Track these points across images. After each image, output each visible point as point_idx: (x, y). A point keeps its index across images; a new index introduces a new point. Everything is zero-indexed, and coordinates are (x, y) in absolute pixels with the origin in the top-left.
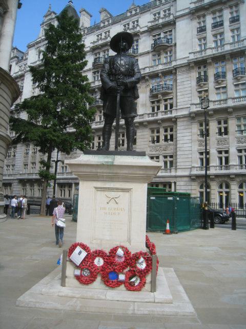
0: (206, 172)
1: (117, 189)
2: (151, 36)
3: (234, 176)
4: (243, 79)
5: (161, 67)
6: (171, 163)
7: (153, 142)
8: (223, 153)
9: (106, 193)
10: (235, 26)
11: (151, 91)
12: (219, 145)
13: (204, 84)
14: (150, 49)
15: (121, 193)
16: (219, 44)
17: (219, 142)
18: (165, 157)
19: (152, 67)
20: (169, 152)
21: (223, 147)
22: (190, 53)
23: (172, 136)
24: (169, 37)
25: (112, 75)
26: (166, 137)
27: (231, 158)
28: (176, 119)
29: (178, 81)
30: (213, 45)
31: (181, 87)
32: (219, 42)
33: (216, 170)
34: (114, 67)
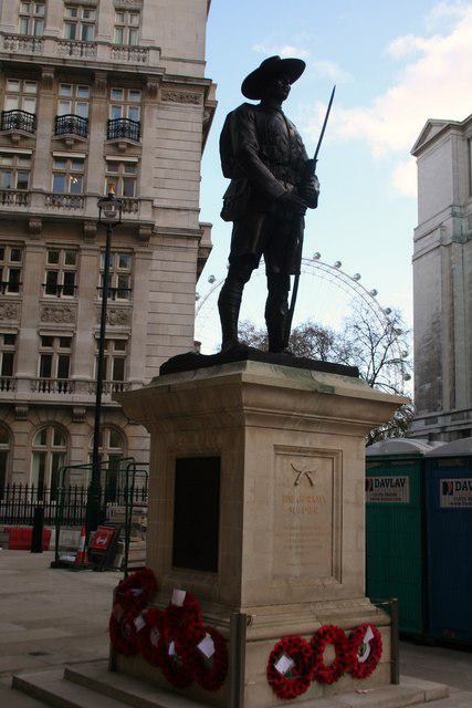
0: (99, 398)
3: (83, 411)
4: (132, 151)
8: (57, 343)
9: (293, 461)
12: (47, 321)
16: (79, 37)
17: (47, 312)
21: (57, 328)
23: (70, 276)
27: (21, 356)
30: (64, 33)
32: (79, 29)
33: (33, 390)
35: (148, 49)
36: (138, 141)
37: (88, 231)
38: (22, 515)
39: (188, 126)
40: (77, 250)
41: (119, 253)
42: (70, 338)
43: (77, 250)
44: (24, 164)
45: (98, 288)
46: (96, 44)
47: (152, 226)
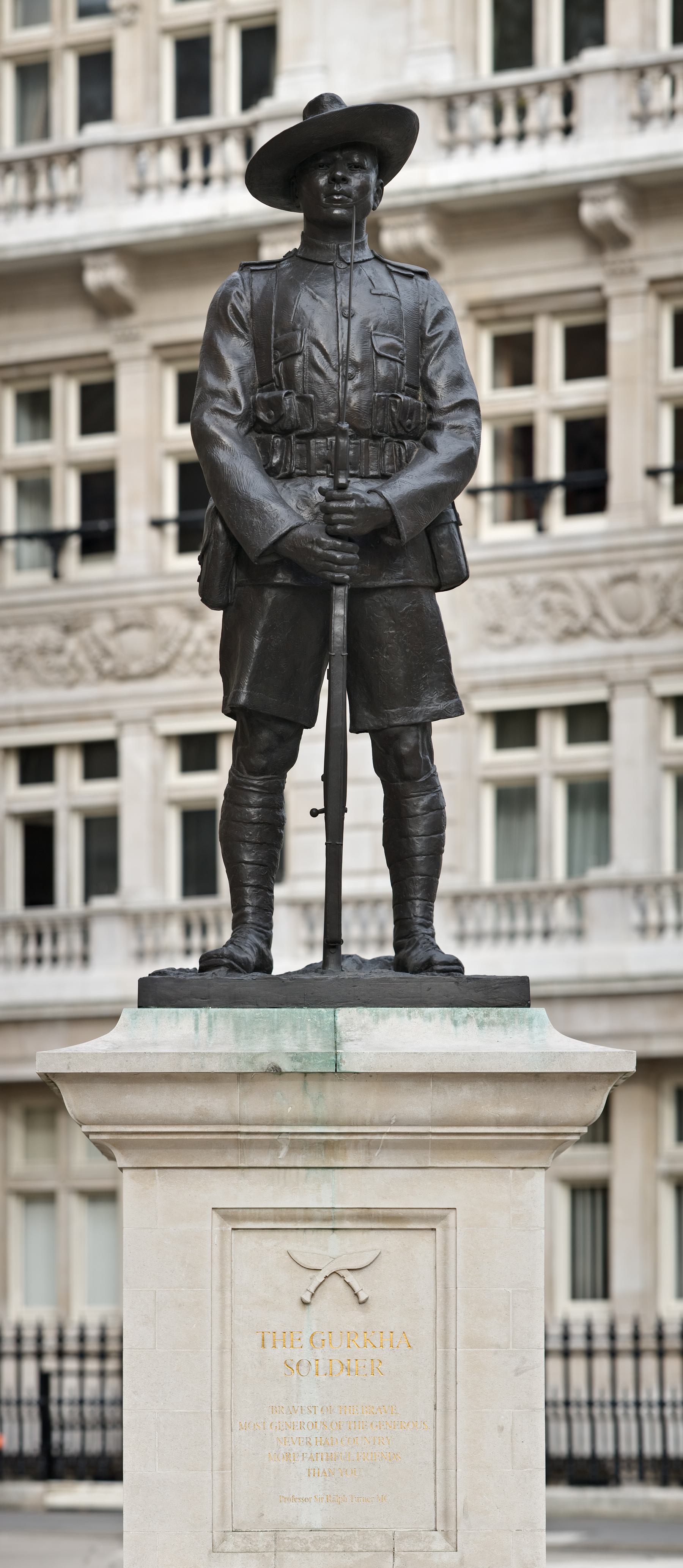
8: (552, 731)
15: (387, 1242)
25: (285, 433)
34: (289, 372)
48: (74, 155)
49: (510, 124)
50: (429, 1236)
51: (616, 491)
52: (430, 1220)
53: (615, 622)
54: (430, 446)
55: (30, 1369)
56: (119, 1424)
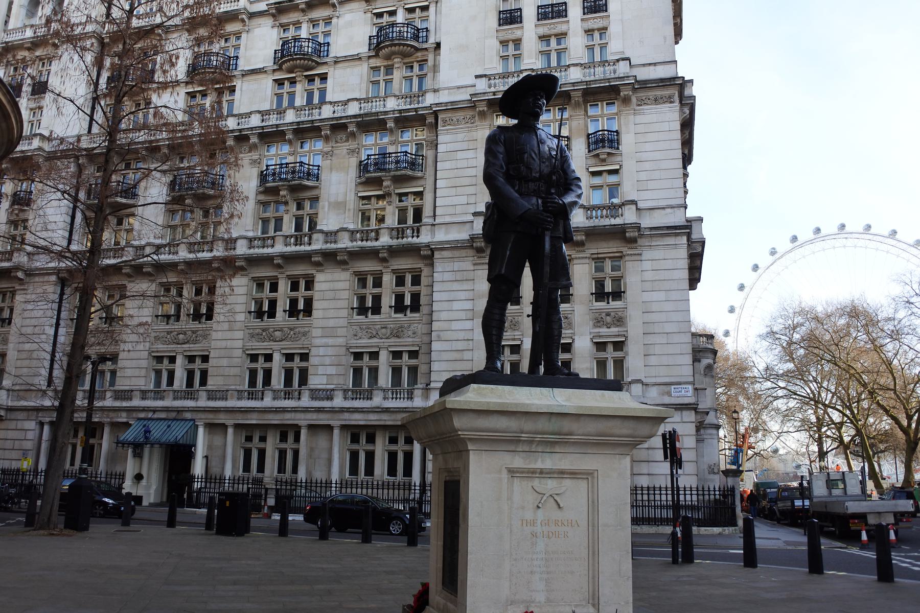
1: (562, 474)
2: (369, 15)
5: (392, 104)
6: (413, 370)
7: (259, 314)
9: (536, 483)
10: (595, 22)
11: (363, 167)
13: (609, 154)
14: (366, 49)
15: (568, 483)
18: (191, 359)
19: (367, 100)
20: (406, 343)
22: (477, 77)
23: (416, 297)
24: (321, 39)
26: (400, 298)
28: (432, 251)
29: (441, 148)
31: (447, 165)
32: (554, 56)
35: (618, 61)
36: (618, 148)
37: (630, 238)
38: (652, 515)
39: (666, 126)
40: (621, 257)
41: (610, 258)
42: (570, 344)
43: (621, 257)
44: (612, 179)
45: (592, 294)
46: (569, 66)
47: (638, 227)
48: (273, 238)
49: (415, 234)
50: (585, 481)
51: (383, 310)
52: (588, 475)
53: (59, 16)
54: (384, 155)
55: (245, 486)
56: (632, 506)
